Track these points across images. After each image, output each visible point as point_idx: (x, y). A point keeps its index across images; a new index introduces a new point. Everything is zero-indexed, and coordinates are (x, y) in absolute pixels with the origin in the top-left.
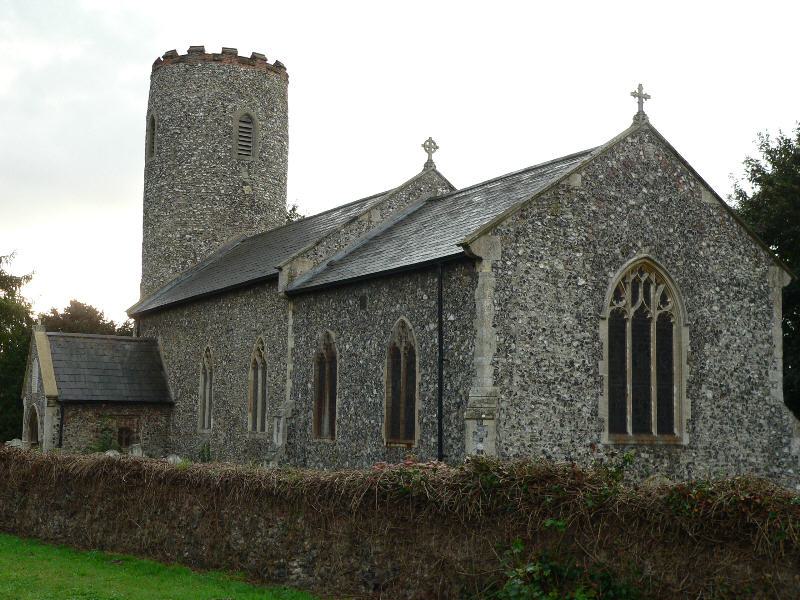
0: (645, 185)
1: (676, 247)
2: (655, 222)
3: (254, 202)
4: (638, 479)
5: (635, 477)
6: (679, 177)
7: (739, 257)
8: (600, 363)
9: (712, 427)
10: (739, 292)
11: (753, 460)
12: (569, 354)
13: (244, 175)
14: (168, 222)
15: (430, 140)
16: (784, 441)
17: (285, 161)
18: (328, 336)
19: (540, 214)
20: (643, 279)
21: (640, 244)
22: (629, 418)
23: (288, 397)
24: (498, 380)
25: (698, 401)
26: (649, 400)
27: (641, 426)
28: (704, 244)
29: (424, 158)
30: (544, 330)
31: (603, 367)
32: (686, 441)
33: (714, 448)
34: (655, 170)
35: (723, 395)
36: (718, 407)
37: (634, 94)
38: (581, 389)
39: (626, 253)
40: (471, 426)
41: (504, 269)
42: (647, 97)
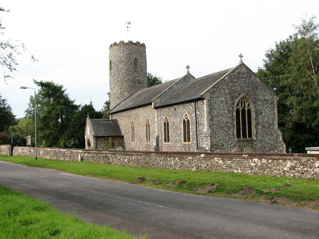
13: (136, 74)
14: (117, 88)
15: (188, 66)
27: (244, 136)
29: (187, 70)
32: (255, 139)
37: (239, 56)
39: (239, 95)
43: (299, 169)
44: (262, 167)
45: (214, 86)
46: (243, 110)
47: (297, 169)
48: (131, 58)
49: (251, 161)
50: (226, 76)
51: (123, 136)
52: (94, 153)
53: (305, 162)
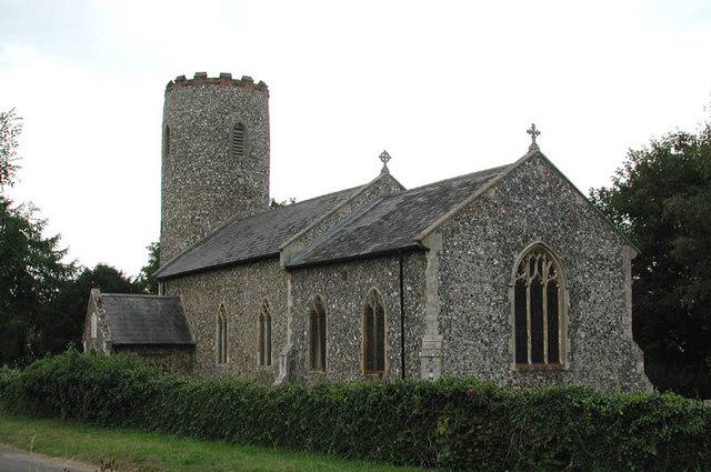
2: (545, 219)
6: (560, 187)
15: (385, 153)
17: (268, 157)
18: (319, 299)
20: (537, 259)
22: (529, 352)
26: (542, 316)
27: (537, 358)
32: (567, 367)
37: (529, 132)
39: (526, 240)
45: (456, 214)
46: (537, 287)
50: (492, 187)
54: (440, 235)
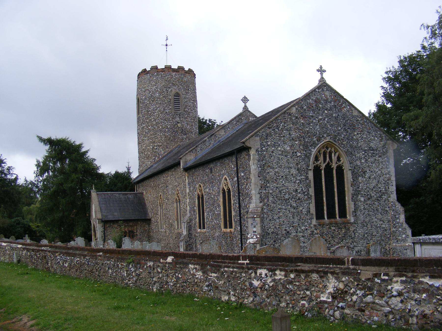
0: (326, 110)
1: (343, 136)
2: (332, 125)
3: (183, 130)
4: (331, 239)
5: (329, 238)
6: (342, 105)
7: (372, 138)
8: (310, 189)
9: (364, 213)
10: (374, 153)
11: (384, 226)
12: (295, 186)
13: (178, 119)
14: (147, 142)
15: (245, 97)
16: (397, 217)
19: (277, 126)
20: (328, 151)
21: (325, 136)
23: (188, 213)
24: (262, 200)
25: (357, 203)
27: (331, 215)
28: (356, 133)
29: (243, 105)
30: (282, 177)
31: (312, 191)
33: (366, 223)
34: (330, 102)
35: (369, 199)
36: (367, 204)
37: (318, 71)
38: (302, 201)
39: (319, 140)
40: (250, 221)
41: (261, 151)
42: (325, 71)
43: (355, 298)
44: (274, 291)
46: (328, 168)
47: (348, 298)
48: (167, 91)
49: (253, 275)
51: (150, 220)
52: (33, 250)
53: (369, 279)
54: (258, 138)
